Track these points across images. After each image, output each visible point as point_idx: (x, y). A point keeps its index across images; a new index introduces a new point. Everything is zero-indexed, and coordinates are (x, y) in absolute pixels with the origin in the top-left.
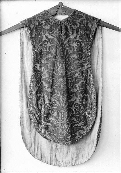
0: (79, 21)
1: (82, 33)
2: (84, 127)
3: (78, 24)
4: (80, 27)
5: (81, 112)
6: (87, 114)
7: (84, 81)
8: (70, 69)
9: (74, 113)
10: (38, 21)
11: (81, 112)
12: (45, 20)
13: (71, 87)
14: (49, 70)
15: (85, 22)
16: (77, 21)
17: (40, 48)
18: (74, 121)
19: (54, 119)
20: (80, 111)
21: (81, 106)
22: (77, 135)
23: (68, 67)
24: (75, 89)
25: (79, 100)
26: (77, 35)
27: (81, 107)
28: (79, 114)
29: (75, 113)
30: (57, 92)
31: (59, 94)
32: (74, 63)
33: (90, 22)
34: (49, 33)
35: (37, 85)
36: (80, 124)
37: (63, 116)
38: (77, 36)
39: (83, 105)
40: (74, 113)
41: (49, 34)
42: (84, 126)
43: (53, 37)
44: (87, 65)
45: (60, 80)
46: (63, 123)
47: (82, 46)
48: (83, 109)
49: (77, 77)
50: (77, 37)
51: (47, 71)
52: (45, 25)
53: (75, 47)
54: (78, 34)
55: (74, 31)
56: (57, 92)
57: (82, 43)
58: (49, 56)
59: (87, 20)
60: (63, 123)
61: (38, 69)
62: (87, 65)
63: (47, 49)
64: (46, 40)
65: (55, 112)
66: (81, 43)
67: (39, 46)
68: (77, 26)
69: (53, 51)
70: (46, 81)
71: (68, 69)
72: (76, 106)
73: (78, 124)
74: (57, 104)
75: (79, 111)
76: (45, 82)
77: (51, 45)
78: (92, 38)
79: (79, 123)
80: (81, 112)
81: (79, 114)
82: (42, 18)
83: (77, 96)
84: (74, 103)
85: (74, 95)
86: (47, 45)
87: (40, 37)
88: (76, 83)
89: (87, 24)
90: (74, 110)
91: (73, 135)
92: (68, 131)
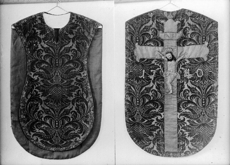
0: (76, 31)
1: (78, 41)
2: (80, 135)
3: (75, 33)
4: (76, 36)
5: (77, 119)
6: (83, 122)
7: (80, 89)
8: (66, 77)
9: (71, 120)
10: (34, 29)
11: (78, 119)
12: (40, 29)
13: (67, 95)
14: (44, 79)
15: (82, 31)
16: (74, 30)
17: (34, 56)
18: (71, 128)
19: (129, 103)
20: (157, 97)
21: (158, 93)
22: (154, 120)
23: (64, 76)
24: (71, 98)
25: (76, 107)
26: (73, 44)
27: (158, 94)
28: (76, 121)
29: (72, 120)
30: (52, 100)
31: (53, 102)
32: (71, 72)
33: (87, 31)
34: (44, 42)
35: (30, 93)
36: (157, 110)
37: (57, 124)
38: (73, 45)
39: (160, 92)
40: (71, 120)
41: (45, 43)
42: (162, 112)
43: (48, 47)
44: (83, 74)
45: (55, 89)
46: (57, 130)
47: (78, 54)
48: (79, 116)
49: (74, 85)
50: (73, 46)
51: (41, 79)
52: (40, 34)
53: (71, 56)
54: (154, 22)
55: (70, 40)
56: (52, 100)
57: (78, 52)
58: (44, 65)
59: (84, 29)
60: (138, 108)
61: (32, 77)
62: (83, 74)
63: (42, 57)
64: (41, 49)
65: (49, 120)
66: (76, 52)
67: (34, 55)
68: (73, 35)
69: (48, 60)
70: (40, 89)
71: (65, 77)
72: (153, 92)
73: (156, 109)
74: (51, 112)
75: (76, 119)
76: (39, 90)
77: (46, 54)
78: (88, 47)
79: (76, 130)
80: (78, 119)
81: (157, 100)
82: (38, 27)
83: (73, 104)
84: (71, 111)
85: (70, 103)
86: (42, 54)
87: (35, 46)
88: (72, 91)
89: (83, 33)
90: (71, 117)
91: (150, 120)
92: (62, 138)
